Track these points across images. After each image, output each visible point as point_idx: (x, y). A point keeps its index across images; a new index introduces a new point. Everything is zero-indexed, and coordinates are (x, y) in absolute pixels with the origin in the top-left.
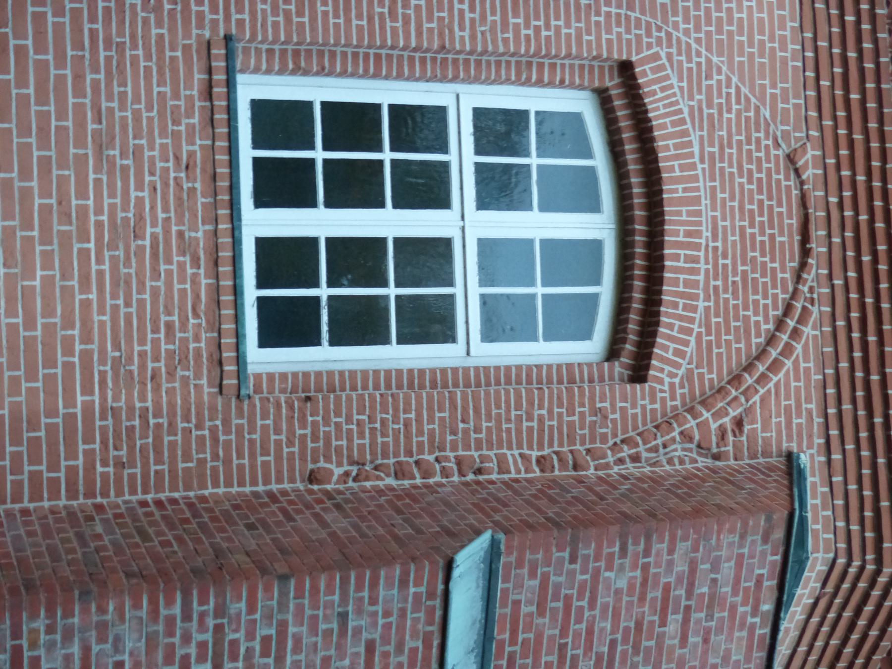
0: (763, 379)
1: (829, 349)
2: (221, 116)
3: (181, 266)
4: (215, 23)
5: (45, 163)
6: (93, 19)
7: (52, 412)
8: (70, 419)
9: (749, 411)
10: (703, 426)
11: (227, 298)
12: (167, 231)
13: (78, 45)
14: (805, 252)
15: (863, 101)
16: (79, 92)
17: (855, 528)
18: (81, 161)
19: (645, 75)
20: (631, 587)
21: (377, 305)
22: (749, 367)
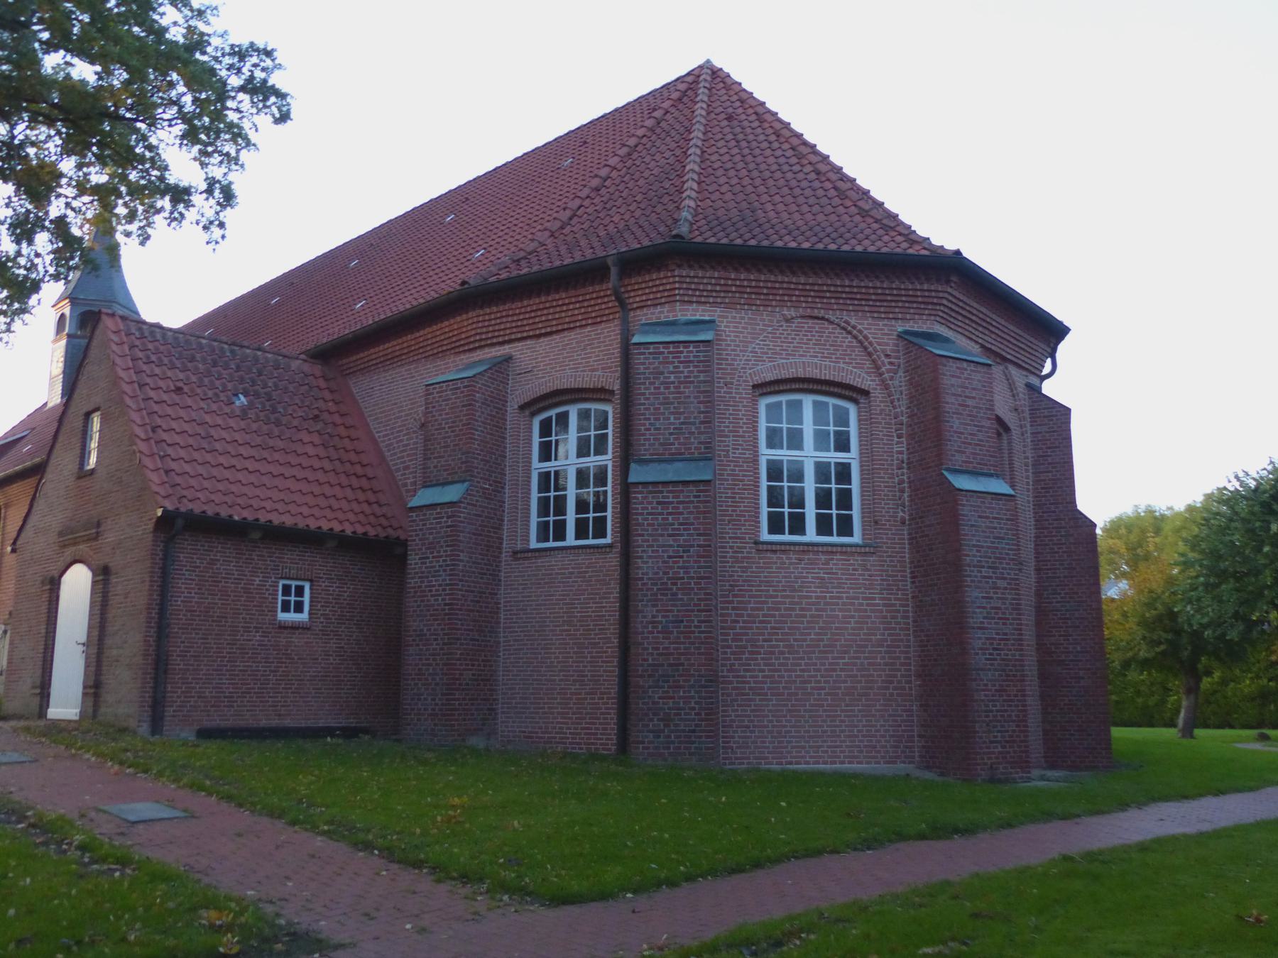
0: (870, 343)
1: (860, 314)
2: (783, 547)
3: (834, 564)
4: (750, 548)
5: (802, 609)
6: (751, 591)
7: (881, 611)
8: (884, 605)
9: (883, 351)
10: (889, 371)
11: (844, 549)
12: (822, 569)
13: (760, 596)
14: (823, 318)
15: (767, 288)
16: (777, 596)
17: (927, 312)
18: (800, 597)
19: (758, 379)
20: (959, 419)
21: (839, 491)
22: (866, 348)
